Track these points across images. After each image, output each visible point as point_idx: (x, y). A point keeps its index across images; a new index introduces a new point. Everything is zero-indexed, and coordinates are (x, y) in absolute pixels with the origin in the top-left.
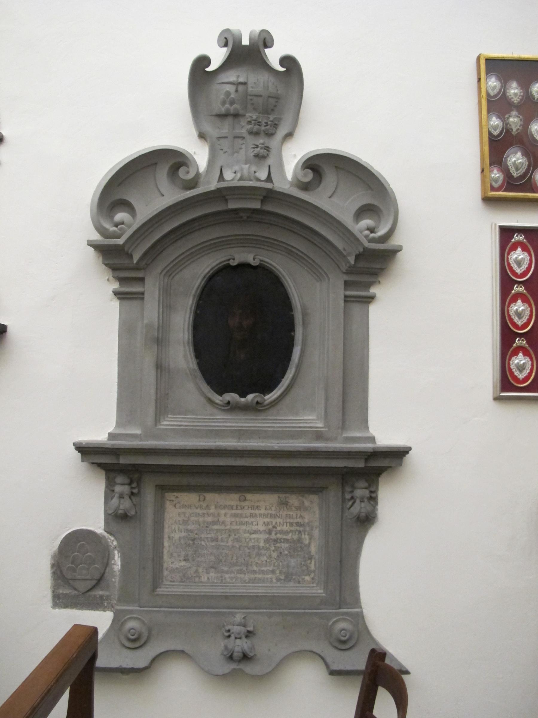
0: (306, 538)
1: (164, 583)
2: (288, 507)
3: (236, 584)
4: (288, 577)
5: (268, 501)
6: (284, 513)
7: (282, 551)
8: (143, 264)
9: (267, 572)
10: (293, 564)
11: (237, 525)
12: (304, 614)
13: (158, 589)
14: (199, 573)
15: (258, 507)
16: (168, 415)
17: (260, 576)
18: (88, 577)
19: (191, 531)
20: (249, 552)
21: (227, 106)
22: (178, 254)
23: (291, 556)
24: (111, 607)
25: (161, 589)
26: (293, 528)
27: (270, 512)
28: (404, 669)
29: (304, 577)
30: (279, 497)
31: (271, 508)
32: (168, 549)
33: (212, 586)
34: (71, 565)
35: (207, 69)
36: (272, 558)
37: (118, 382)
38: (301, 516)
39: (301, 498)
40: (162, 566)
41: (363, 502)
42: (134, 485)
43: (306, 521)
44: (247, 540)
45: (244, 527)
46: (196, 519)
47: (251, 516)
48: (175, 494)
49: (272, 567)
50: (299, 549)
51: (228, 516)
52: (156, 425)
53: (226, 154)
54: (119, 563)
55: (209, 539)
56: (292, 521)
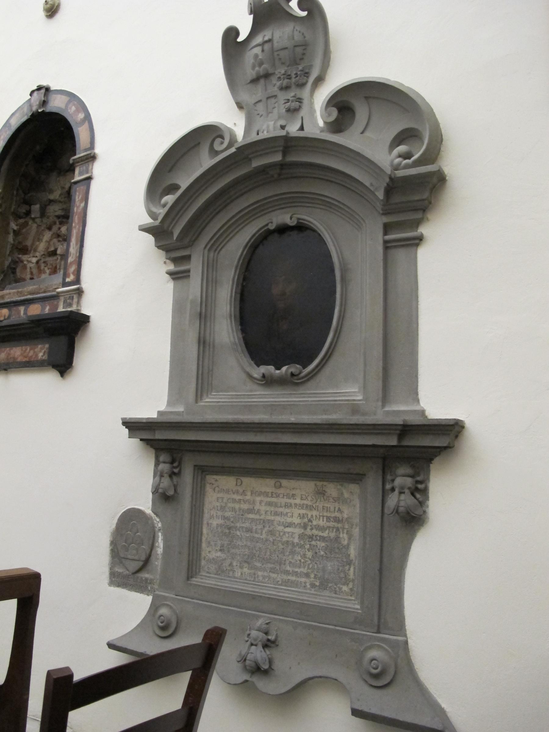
0: (344, 536)
1: (201, 574)
2: (325, 497)
4: (324, 585)
5: (304, 488)
7: (317, 551)
8: (186, 241)
13: (194, 579)
14: (233, 566)
16: (212, 392)
17: (294, 578)
18: (136, 558)
19: (227, 518)
20: (283, 549)
21: (257, 68)
22: (219, 227)
26: (331, 524)
27: (305, 502)
29: (341, 586)
30: (316, 485)
31: (307, 498)
32: (206, 536)
35: (240, 39)
37: (170, 362)
38: (339, 510)
39: (339, 487)
40: (200, 554)
41: (404, 493)
42: (175, 464)
43: (345, 516)
44: (281, 534)
45: (278, 518)
47: (287, 506)
48: (215, 477)
49: (306, 568)
50: (337, 551)
51: (263, 504)
52: (196, 402)
53: (262, 117)
55: (244, 530)
56: (329, 515)
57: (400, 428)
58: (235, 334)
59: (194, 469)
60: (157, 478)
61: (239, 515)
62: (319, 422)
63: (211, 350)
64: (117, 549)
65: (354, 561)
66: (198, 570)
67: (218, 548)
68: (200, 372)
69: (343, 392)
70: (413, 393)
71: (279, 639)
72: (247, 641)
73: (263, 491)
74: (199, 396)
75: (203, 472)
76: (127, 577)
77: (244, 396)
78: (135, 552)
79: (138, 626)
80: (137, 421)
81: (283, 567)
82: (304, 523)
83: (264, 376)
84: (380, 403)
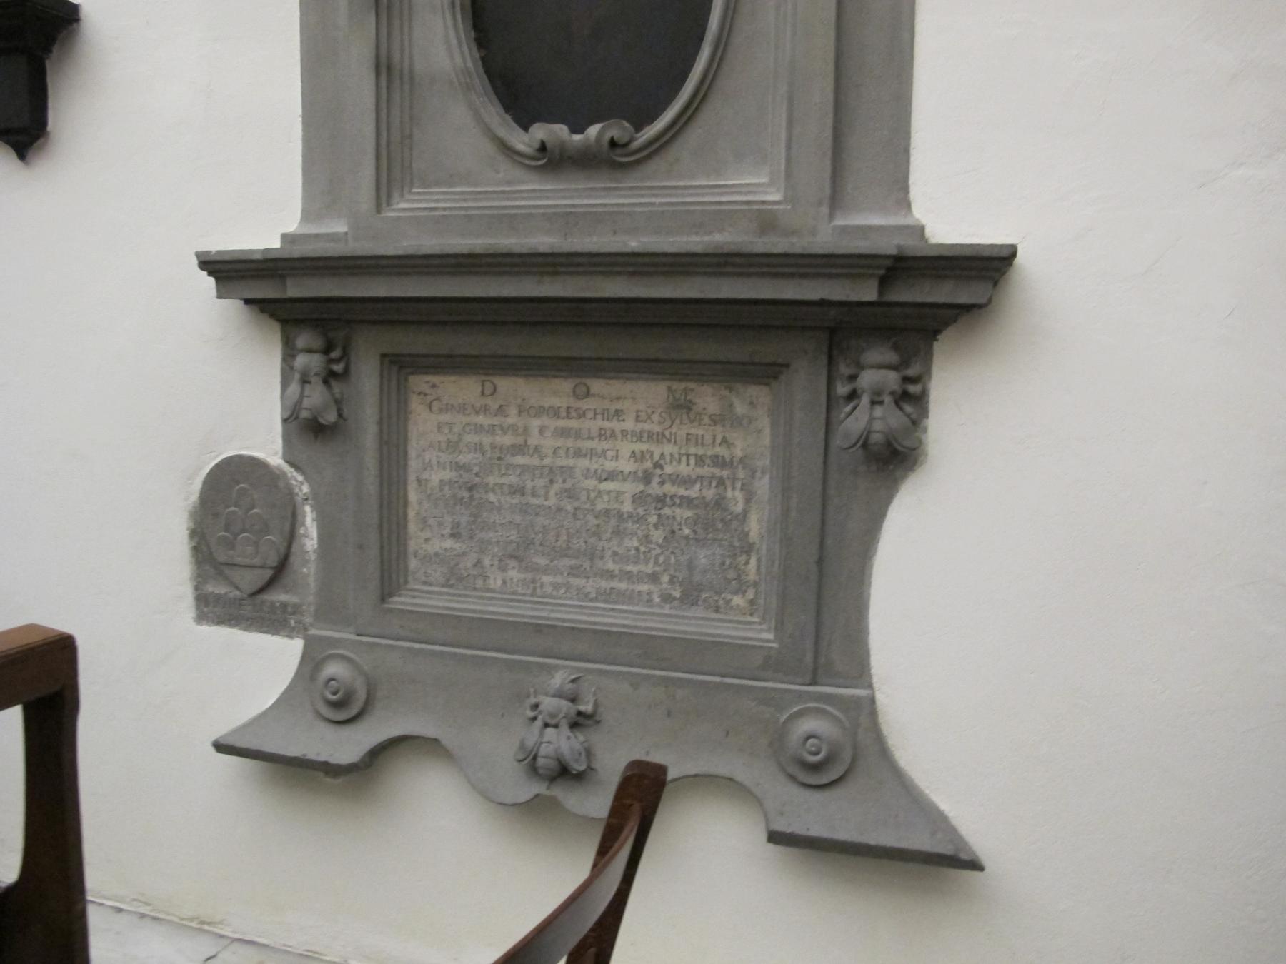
2: (692, 415)
3: (567, 601)
4: (691, 596)
5: (649, 395)
6: (681, 430)
7: (676, 528)
9: (639, 578)
10: (703, 561)
11: (567, 456)
12: (718, 686)
13: (396, 599)
14: (482, 567)
15: (618, 413)
16: (412, 185)
17: (623, 586)
18: (256, 561)
20: (598, 526)
23: (697, 540)
25: (402, 599)
26: (706, 471)
27: (647, 426)
28: (963, 856)
29: (729, 597)
30: (669, 389)
31: (649, 417)
33: (512, 600)
36: (651, 542)
38: (724, 441)
39: (725, 393)
40: (405, 545)
41: (881, 403)
42: (335, 354)
44: (593, 495)
45: (584, 463)
46: (476, 439)
47: (602, 435)
49: (651, 565)
50: (720, 526)
51: (548, 434)
52: (378, 209)
55: (506, 490)
56: (701, 452)
57: (888, 263)
58: (466, 49)
59: (382, 364)
60: (294, 388)
61: (490, 459)
62: (698, 249)
63: (407, 87)
64: (208, 546)
65: (757, 546)
66: (402, 580)
67: (447, 531)
68: (383, 142)
69: (733, 185)
70: (897, 187)
71: (601, 709)
72: (535, 718)
73: (547, 405)
74: (384, 198)
75: (401, 368)
76: (238, 602)
77: (485, 191)
78: (250, 549)
79: (278, 701)
80: (236, 257)
81: (599, 564)
82: (646, 471)
83: (543, 148)
84: (825, 210)
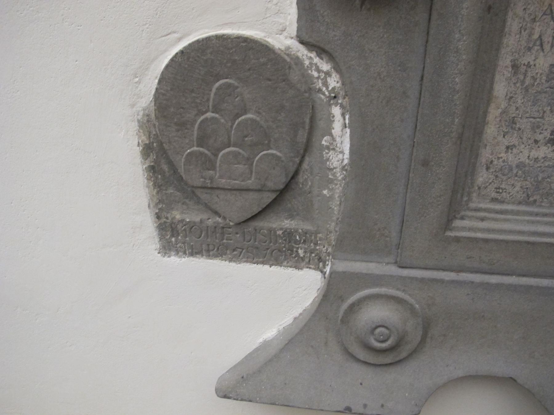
1: (472, 205)
13: (458, 223)
18: (251, 183)
24: (318, 262)
25: (466, 223)
34: (195, 148)
54: (344, 142)
64: (170, 163)
